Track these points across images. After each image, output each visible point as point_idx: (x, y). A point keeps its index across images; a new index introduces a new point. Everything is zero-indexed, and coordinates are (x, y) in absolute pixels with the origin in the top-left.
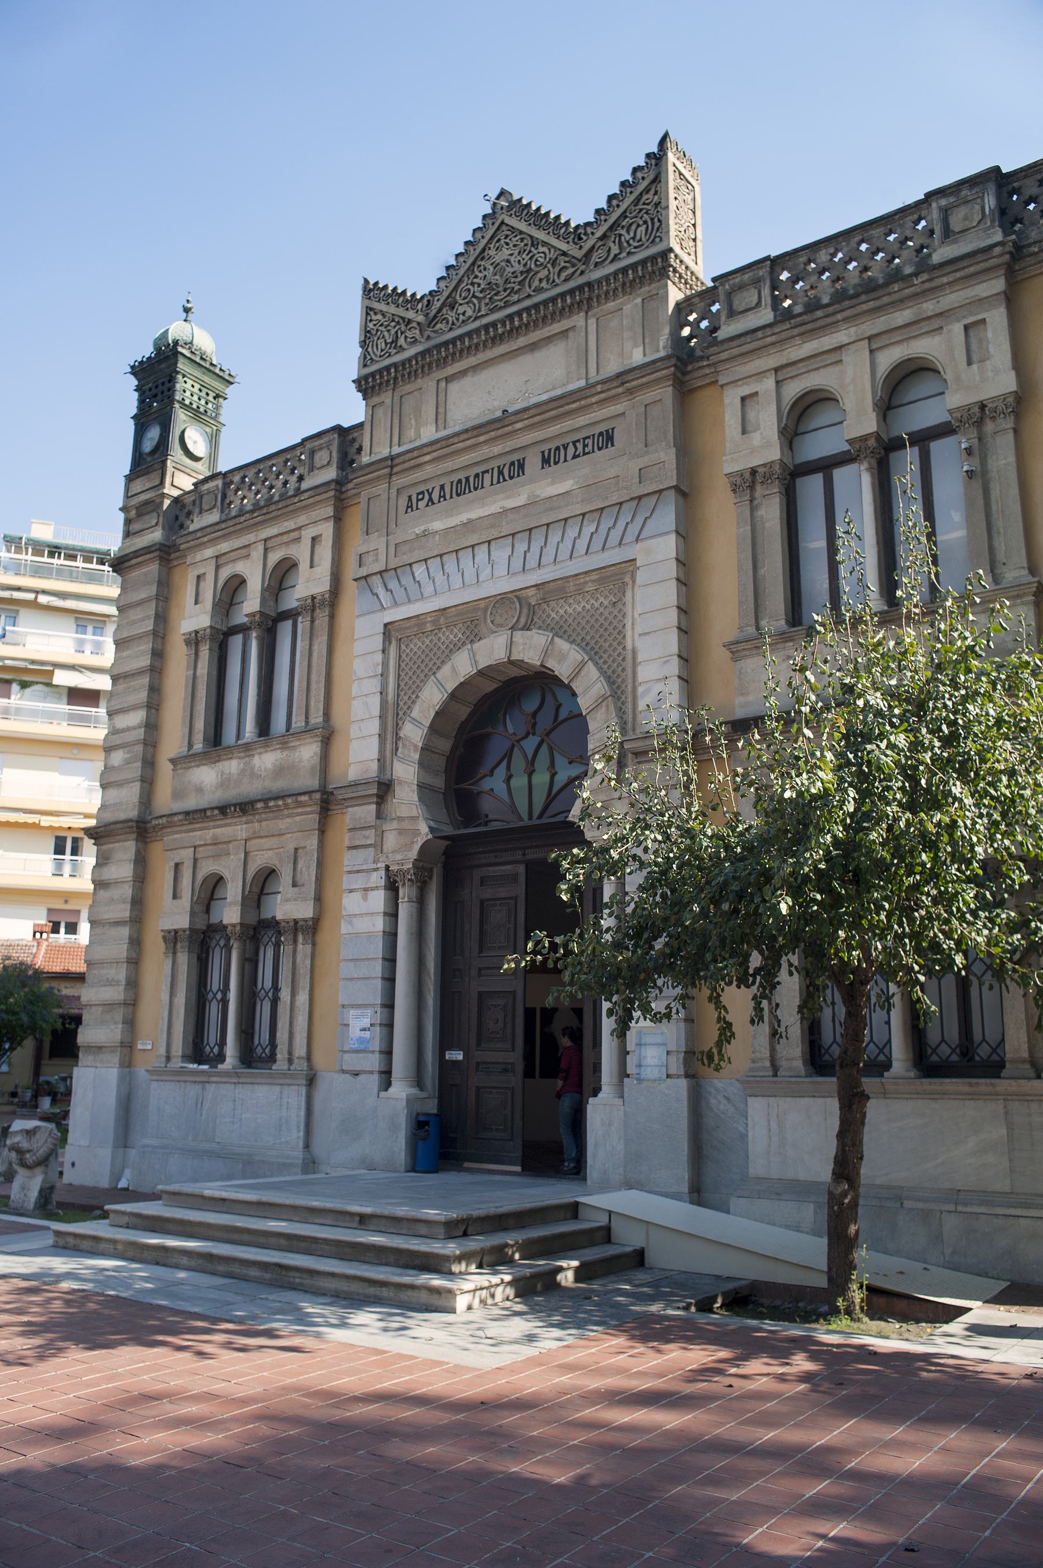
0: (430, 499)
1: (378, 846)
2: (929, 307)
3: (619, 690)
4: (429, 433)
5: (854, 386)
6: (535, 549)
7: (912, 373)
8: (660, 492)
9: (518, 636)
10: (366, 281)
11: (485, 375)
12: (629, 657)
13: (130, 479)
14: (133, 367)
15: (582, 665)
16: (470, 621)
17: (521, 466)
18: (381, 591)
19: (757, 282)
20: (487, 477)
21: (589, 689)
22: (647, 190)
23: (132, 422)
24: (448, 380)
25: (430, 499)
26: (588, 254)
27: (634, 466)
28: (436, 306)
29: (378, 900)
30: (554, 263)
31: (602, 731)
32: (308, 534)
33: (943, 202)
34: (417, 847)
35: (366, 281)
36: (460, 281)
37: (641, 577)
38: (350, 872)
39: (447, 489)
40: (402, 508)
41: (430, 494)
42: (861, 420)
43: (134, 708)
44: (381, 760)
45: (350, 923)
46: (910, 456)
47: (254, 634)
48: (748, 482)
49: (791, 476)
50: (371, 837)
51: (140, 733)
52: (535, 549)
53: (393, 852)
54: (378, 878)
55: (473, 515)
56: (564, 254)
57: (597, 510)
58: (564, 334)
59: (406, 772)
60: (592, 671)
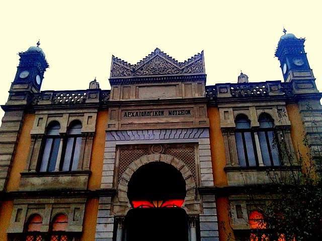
0: (133, 115)
1: (112, 210)
2: (269, 104)
3: (195, 175)
4: (133, 98)
5: (64, 122)
6: (193, 134)
7: (77, 123)
8: (193, 128)
9: (162, 155)
10: (33, 62)
11: (153, 88)
12: (197, 167)
13: (13, 84)
14: (20, 53)
15: (183, 166)
16: (146, 148)
17: (163, 112)
18: (115, 136)
19: (226, 88)
20: (152, 114)
21: (186, 173)
22: (199, 60)
23: (17, 69)
24: (140, 87)
25: (133, 115)
26: (183, 70)
27: (197, 120)
28: (134, 69)
29: (111, 227)
30: (173, 69)
31: (190, 184)
32: (86, 115)
33: (270, 84)
34: (127, 211)
35: (33, 62)
36: (144, 65)
37: (200, 147)
38: (99, 217)
39: (139, 114)
40: (123, 116)
41: (133, 114)
42: (63, 130)
43: (7, 154)
44: (113, 183)
45: (99, 234)
46: (51, 140)
47: (62, 139)
48: (35, 137)
49: (44, 138)
50: (109, 207)
51: (9, 163)
52: (193, 134)
53: (117, 212)
54: (111, 220)
55: (149, 121)
56: (176, 68)
57: (191, 128)
58: (175, 85)
59: (123, 187)
60: (186, 168)
